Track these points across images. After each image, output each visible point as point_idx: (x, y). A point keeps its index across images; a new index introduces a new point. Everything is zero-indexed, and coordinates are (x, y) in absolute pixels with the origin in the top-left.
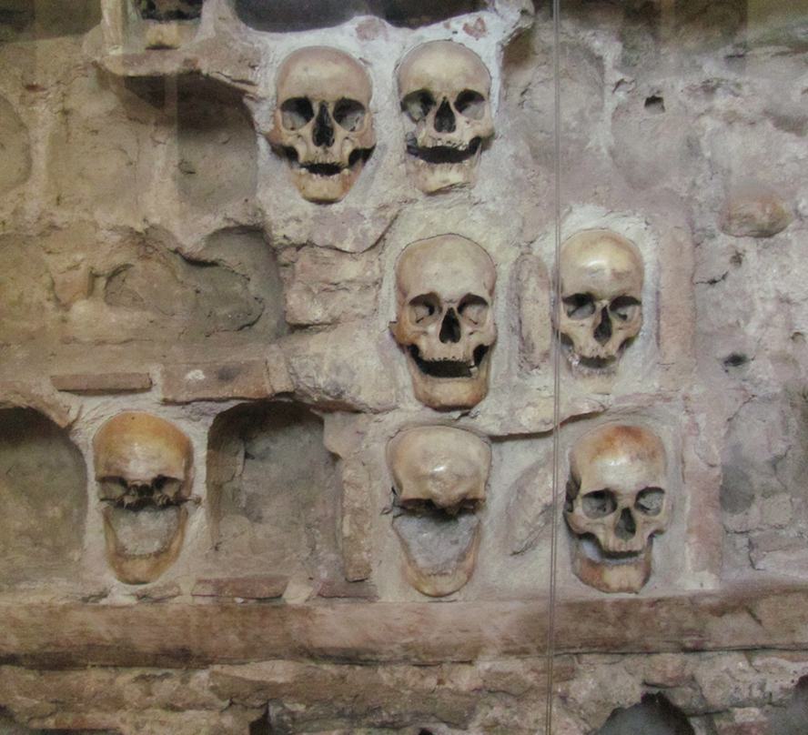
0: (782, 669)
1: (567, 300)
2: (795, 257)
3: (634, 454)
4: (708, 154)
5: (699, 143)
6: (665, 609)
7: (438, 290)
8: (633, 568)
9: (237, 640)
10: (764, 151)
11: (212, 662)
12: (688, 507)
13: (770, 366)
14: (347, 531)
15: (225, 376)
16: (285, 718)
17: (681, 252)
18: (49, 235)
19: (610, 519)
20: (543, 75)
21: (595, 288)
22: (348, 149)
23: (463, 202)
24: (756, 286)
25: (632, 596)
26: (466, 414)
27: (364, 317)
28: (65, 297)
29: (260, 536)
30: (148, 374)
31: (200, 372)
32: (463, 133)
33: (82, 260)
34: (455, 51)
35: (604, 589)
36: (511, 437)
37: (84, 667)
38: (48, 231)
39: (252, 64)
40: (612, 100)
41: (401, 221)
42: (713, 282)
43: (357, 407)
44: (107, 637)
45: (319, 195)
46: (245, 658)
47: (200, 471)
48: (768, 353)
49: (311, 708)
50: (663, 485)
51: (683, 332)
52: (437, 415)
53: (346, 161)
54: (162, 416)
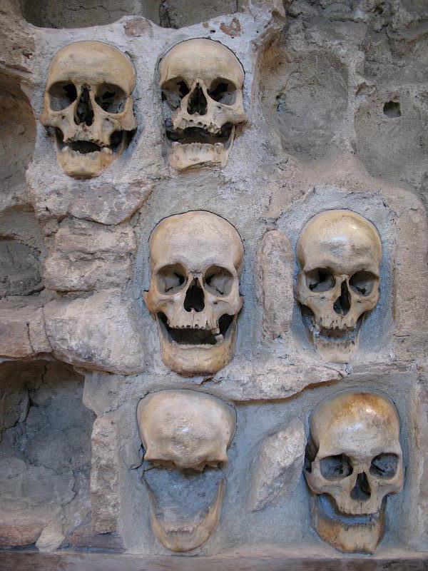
1: (308, 274)
19: (349, 482)
20: (296, 82)
23: (213, 180)
26: (210, 380)
32: (213, 117)
34: (199, 51)
36: (252, 402)
39: (26, 52)
40: (354, 104)
41: (155, 197)
43: (108, 368)
52: (182, 380)
53: (106, 140)
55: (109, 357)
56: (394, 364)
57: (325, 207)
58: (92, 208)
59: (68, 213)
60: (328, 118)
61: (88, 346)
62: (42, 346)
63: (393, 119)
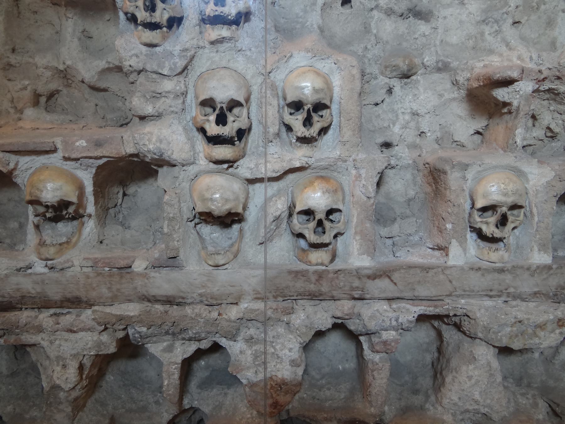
0: (408, 310)
2: (421, 90)
3: (325, 190)
4: (375, 31)
5: (370, 25)
6: (342, 275)
7: (214, 96)
8: (324, 252)
9: (107, 291)
10: (406, 31)
11: (93, 305)
12: (355, 220)
13: (407, 150)
14: (166, 230)
15: (98, 144)
16: (136, 335)
17: (354, 80)
18: (8, 70)
19: (312, 225)
21: (303, 99)
22: (166, 16)
24: (400, 106)
25: (324, 268)
26: (232, 166)
27: (176, 113)
28: (20, 106)
29: (128, 236)
30: (54, 142)
31: (84, 141)
33: (28, 85)
35: (309, 264)
37: (21, 309)
38: (7, 67)
42: (377, 104)
44: (33, 292)
45: (148, 41)
46: (112, 301)
47: (90, 199)
48: (406, 143)
49: (150, 330)
50: (341, 207)
51: (354, 125)
53: (164, 22)
54: (65, 167)
55: (172, 154)
56: (340, 159)
57: (299, 65)
58: (159, 65)
59: (143, 68)
60: (305, 11)
61: (160, 148)
62: (132, 150)
63: (347, 11)
